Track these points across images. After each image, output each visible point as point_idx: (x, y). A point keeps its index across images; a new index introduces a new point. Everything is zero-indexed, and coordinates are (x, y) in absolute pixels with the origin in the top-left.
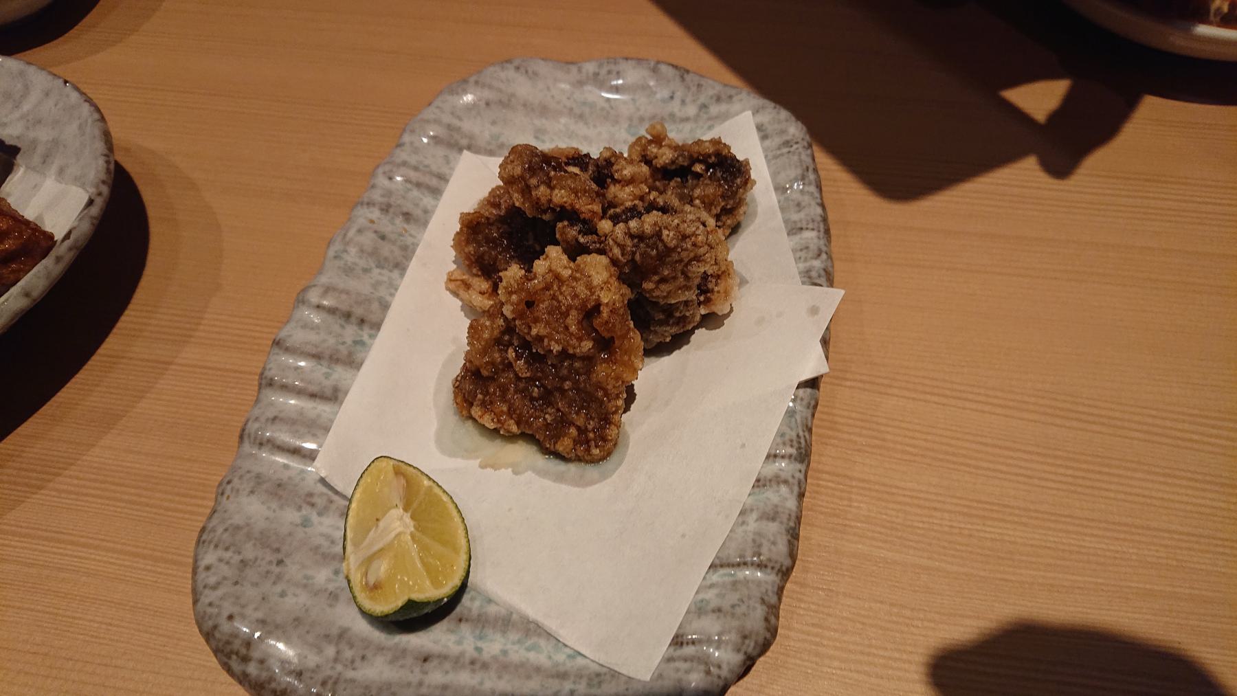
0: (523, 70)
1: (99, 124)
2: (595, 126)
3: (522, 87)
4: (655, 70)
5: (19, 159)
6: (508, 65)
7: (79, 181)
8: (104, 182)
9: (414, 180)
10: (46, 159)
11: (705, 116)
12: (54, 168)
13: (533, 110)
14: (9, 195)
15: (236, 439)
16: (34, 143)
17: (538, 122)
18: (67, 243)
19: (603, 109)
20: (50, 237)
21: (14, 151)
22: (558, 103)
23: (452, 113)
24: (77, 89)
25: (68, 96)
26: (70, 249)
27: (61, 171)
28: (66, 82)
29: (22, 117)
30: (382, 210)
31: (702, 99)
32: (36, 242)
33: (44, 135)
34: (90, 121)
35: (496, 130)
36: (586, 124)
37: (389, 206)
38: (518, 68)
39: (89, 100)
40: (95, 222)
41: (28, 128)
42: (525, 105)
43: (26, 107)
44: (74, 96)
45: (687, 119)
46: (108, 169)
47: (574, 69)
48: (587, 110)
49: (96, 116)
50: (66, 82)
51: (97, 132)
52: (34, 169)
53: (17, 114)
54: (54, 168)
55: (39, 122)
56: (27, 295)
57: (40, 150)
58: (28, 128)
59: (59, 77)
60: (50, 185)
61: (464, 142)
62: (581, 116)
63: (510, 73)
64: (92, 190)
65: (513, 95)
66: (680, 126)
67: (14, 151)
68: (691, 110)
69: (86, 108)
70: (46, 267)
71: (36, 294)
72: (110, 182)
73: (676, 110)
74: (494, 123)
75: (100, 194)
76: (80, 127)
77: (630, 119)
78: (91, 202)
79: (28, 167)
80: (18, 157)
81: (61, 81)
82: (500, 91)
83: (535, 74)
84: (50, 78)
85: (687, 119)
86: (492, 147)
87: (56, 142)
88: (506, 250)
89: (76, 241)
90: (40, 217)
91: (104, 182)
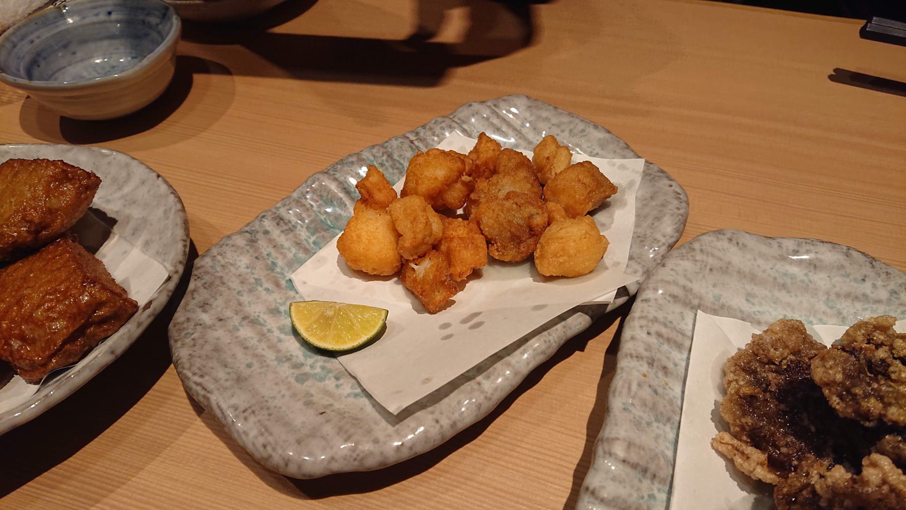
0: (735, 242)
1: (181, 214)
2: (796, 295)
3: (735, 256)
4: (847, 255)
5: (116, 229)
6: (721, 236)
7: (160, 255)
8: (180, 262)
9: (665, 336)
10: (135, 232)
11: (897, 302)
12: (140, 242)
13: (745, 277)
16: (128, 218)
17: (749, 287)
18: (148, 311)
19: (802, 281)
20: (135, 306)
21: (113, 222)
22: (764, 271)
23: (685, 276)
24: (166, 182)
25: (158, 186)
26: (149, 316)
27: (147, 244)
28: (159, 176)
29: (123, 197)
30: (649, 364)
31: (892, 286)
32: (124, 309)
33: (136, 213)
34: (173, 211)
35: (717, 291)
36: (788, 292)
37: (653, 360)
38: (730, 240)
39: (174, 192)
40: (170, 294)
41: (125, 206)
42: (739, 272)
43: (126, 190)
44: (164, 188)
45: (879, 301)
46: (185, 251)
47: (774, 243)
48: (789, 281)
49: (179, 206)
50: (159, 176)
52: (125, 238)
53: (118, 195)
54: (140, 242)
55: (134, 202)
56: (112, 352)
57: (132, 224)
58: (125, 206)
59: (154, 171)
60: (136, 255)
61: (696, 302)
62: (784, 286)
63: (723, 244)
64: (171, 268)
65: (729, 263)
66: (875, 306)
67: (113, 222)
68: (883, 294)
69: (172, 198)
70: (129, 331)
72: (185, 262)
73: (868, 292)
74: (714, 286)
75: (176, 272)
76: (165, 212)
77: (828, 293)
78: (169, 278)
79: (121, 237)
80: (115, 227)
81: (154, 174)
82: (720, 259)
83: (744, 246)
84: (147, 171)
85: (879, 301)
86: (716, 307)
87: (144, 220)
88: (783, 425)
89: (155, 310)
90: (126, 280)
91: (180, 262)
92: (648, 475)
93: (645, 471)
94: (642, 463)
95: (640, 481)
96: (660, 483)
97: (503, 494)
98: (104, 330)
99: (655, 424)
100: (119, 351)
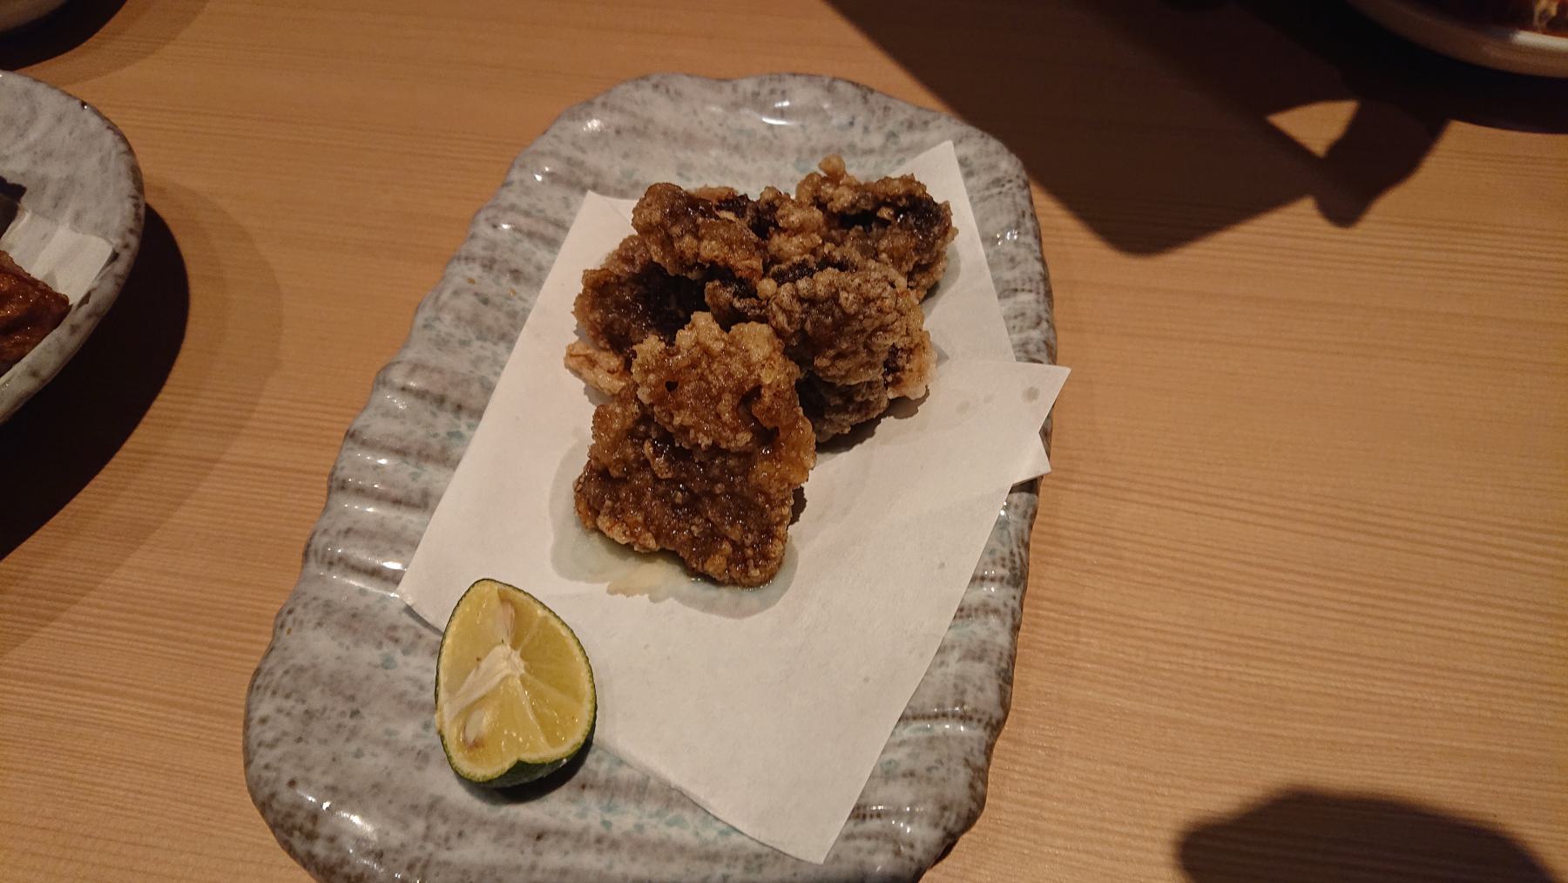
0: (662, 89)
1: (126, 157)
2: (754, 160)
3: (662, 111)
4: (830, 89)
5: (25, 202)
6: (644, 83)
7: (100, 229)
8: (131, 231)
9: (525, 228)
10: (58, 201)
11: (894, 148)
12: (69, 214)
13: (675, 139)
14: (11, 247)
16: (44, 181)
17: (681, 155)
18: (86, 308)
19: (764, 138)
21: (18, 191)
22: (708, 130)
23: (573, 144)
24: (98, 113)
25: (86, 122)
26: (89, 316)
27: (77, 217)
28: (83, 104)
29: (28, 149)
30: (484, 266)
31: (890, 126)
33: (55, 171)
34: (114, 153)
35: (628, 164)
36: (743, 157)
37: (493, 261)
38: (656, 87)
39: (112, 127)
40: (121, 281)
41: (35, 163)
42: (665, 134)
43: (33, 136)
44: (94, 121)
45: (871, 151)
46: (137, 214)
47: (728, 87)
48: (744, 140)
49: (122, 147)
50: (83, 104)
51: (123, 168)
52: (43, 214)
53: (21, 145)
54: (69, 214)
55: (50, 154)
56: (34, 374)
57: (51, 190)
58: (35, 163)
59: (75, 98)
60: (63, 235)
61: (588, 180)
62: (736, 148)
63: (646, 92)
64: (117, 241)
65: (650, 121)
66: (863, 160)
67: (18, 191)
68: (876, 140)
69: (109, 137)
70: (58, 339)
72: (139, 230)
73: (857, 140)
74: (626, 156)
75: (126, 246)
76: (102, 161)
77: (799, 151)
78: (115, 257)
79: (35, 212)
80: (23, 199)
81: (77, 103)
82: (634, 115)
83: (679, 94)
84: (63, 98)
85: (871, 151)
86: (624, 187)
87: (70, 180)
89: (97, 305)
90: (51, 275)
91: (131, 231)
92: (448, 405)
93: (441, 401)
94: (436, 389)
95: (434, 414)
96: (471, 416)
97: (1392, 604)
98: (17, 344)
99: (477, 344)
100: (45, 372)
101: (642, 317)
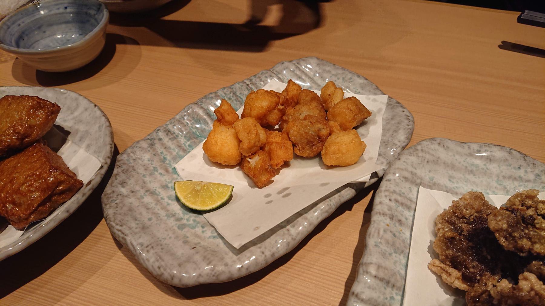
0: (442, 145)
1: (109, 128)
2: (479, 177)
3: (442, 154)
5: (70, 137)
6: (433, 142)
7: (96, 153)
8: (109, 157)
10: (81, 139)
11: (540, 181)
12: (84, 145)
13: (448, 166)
14: (63, 154)
15: (272, 204)
16: (77, 131)
17: (450, 172)
18: (89, 187)
19: (483, 169)
21: (68, 133)
22: (460, 163)
23: (412, 166)
24: (100, 109)
25: (95, 112)
26: (90, 190)
27: (88, 146)
28: (95, 106)
29: (74, 118)
31: (537, 172)
33: (82, 128)
34: (104, 126)
35: (431, 175)
36: (474, 175)
38: (439, 144)
39: (105, 115)
40: (102, 176)
41: (75, 123)
42: (444, 163)
43: (76, 114)
44: (98, 113)
45: (529, 181)
46: (111, 151)
47: (466, 146)
48: (474, 169)
49: (108, 124)
50: (95, 106)
51: (108, 133)
52: (75, 143)
53: (71, 117)
54: (84, 145)
55: (81, 121)
56: (68, 211)
57: (79, 135)
58: (75, 123)
59: (93, 103)
60: (82, 153)
61: (418, 181)
62: (471, 172)
63: (435, 146)
64: (103, 161)
65: (439, 158)
66: (526, 184)
67: (68, 133)
68: (531, 177)
69: (103, 119)
70: (78, 199)
71: (72, 211)
72: (111, 157)
73: (522, 175)
74: (430, 171)
75: (106, 163)
76: (99, 127)
77: (498, 176)
78: (102, 167)
79: (73, 142)
80: (69, 136)
81: (93, 105)
82: (433, 155)
83: (448, 147)
84: (88, 102)
85: (529, 181)
86: (431, 184)
87: (87, 132)
89: (93, 186)
90: (76, 168)
91: (109, 157)
98: (63, 198)
101: (471, 255)
